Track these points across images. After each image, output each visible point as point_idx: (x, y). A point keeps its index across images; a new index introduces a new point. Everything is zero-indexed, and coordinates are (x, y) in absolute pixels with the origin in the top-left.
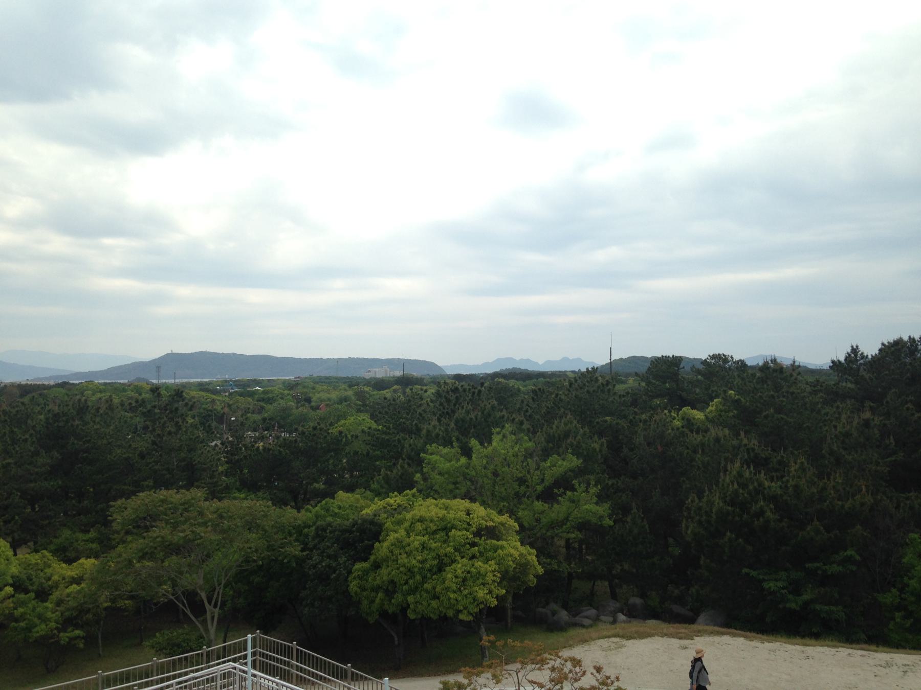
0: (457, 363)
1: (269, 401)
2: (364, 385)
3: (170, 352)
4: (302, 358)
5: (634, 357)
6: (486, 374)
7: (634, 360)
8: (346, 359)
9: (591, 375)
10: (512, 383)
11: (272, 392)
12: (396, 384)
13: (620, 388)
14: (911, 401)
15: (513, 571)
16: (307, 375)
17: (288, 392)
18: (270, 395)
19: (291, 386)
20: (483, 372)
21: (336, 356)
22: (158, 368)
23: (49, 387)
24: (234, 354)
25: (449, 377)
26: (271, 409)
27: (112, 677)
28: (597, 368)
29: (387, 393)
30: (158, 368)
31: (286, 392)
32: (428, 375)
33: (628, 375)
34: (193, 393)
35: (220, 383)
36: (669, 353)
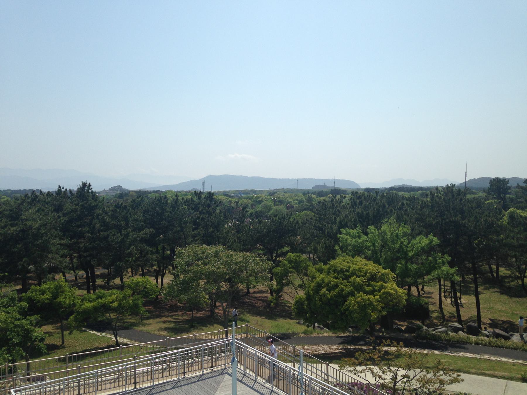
0: (226, 174)
1: (260, 202)
2: (312, 194)
3: (209, 175)
4: (249, 176)
5: (483, 178)
6: (385, 188)
7: (483, 179)
8: (302, 179)
9: (450, 190)
10: (401, 193)
11: (260, 197)
12: (330, 194)
13: (469, 196)
14: (314, 201)
15: (23, 333)
16: (280, 187)
17: (270, 197)
18: (260, 199)
19: (272, 194)
20: (383, 187)
21: (339, 179)
22: (203, 183)
23: (150, 193)
24: (242, 176)
25: (362, 189)
26: (259, 208)
27: (62, 359)
28: (455, 185)
29: (326, 198)
30: (203, 183)
31: (268, 197)
32: (350, 188)
33: (478, 189)
34: (220, 197)
35: (234, 192)
36: (501, 176)
